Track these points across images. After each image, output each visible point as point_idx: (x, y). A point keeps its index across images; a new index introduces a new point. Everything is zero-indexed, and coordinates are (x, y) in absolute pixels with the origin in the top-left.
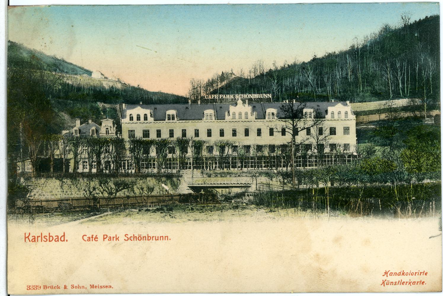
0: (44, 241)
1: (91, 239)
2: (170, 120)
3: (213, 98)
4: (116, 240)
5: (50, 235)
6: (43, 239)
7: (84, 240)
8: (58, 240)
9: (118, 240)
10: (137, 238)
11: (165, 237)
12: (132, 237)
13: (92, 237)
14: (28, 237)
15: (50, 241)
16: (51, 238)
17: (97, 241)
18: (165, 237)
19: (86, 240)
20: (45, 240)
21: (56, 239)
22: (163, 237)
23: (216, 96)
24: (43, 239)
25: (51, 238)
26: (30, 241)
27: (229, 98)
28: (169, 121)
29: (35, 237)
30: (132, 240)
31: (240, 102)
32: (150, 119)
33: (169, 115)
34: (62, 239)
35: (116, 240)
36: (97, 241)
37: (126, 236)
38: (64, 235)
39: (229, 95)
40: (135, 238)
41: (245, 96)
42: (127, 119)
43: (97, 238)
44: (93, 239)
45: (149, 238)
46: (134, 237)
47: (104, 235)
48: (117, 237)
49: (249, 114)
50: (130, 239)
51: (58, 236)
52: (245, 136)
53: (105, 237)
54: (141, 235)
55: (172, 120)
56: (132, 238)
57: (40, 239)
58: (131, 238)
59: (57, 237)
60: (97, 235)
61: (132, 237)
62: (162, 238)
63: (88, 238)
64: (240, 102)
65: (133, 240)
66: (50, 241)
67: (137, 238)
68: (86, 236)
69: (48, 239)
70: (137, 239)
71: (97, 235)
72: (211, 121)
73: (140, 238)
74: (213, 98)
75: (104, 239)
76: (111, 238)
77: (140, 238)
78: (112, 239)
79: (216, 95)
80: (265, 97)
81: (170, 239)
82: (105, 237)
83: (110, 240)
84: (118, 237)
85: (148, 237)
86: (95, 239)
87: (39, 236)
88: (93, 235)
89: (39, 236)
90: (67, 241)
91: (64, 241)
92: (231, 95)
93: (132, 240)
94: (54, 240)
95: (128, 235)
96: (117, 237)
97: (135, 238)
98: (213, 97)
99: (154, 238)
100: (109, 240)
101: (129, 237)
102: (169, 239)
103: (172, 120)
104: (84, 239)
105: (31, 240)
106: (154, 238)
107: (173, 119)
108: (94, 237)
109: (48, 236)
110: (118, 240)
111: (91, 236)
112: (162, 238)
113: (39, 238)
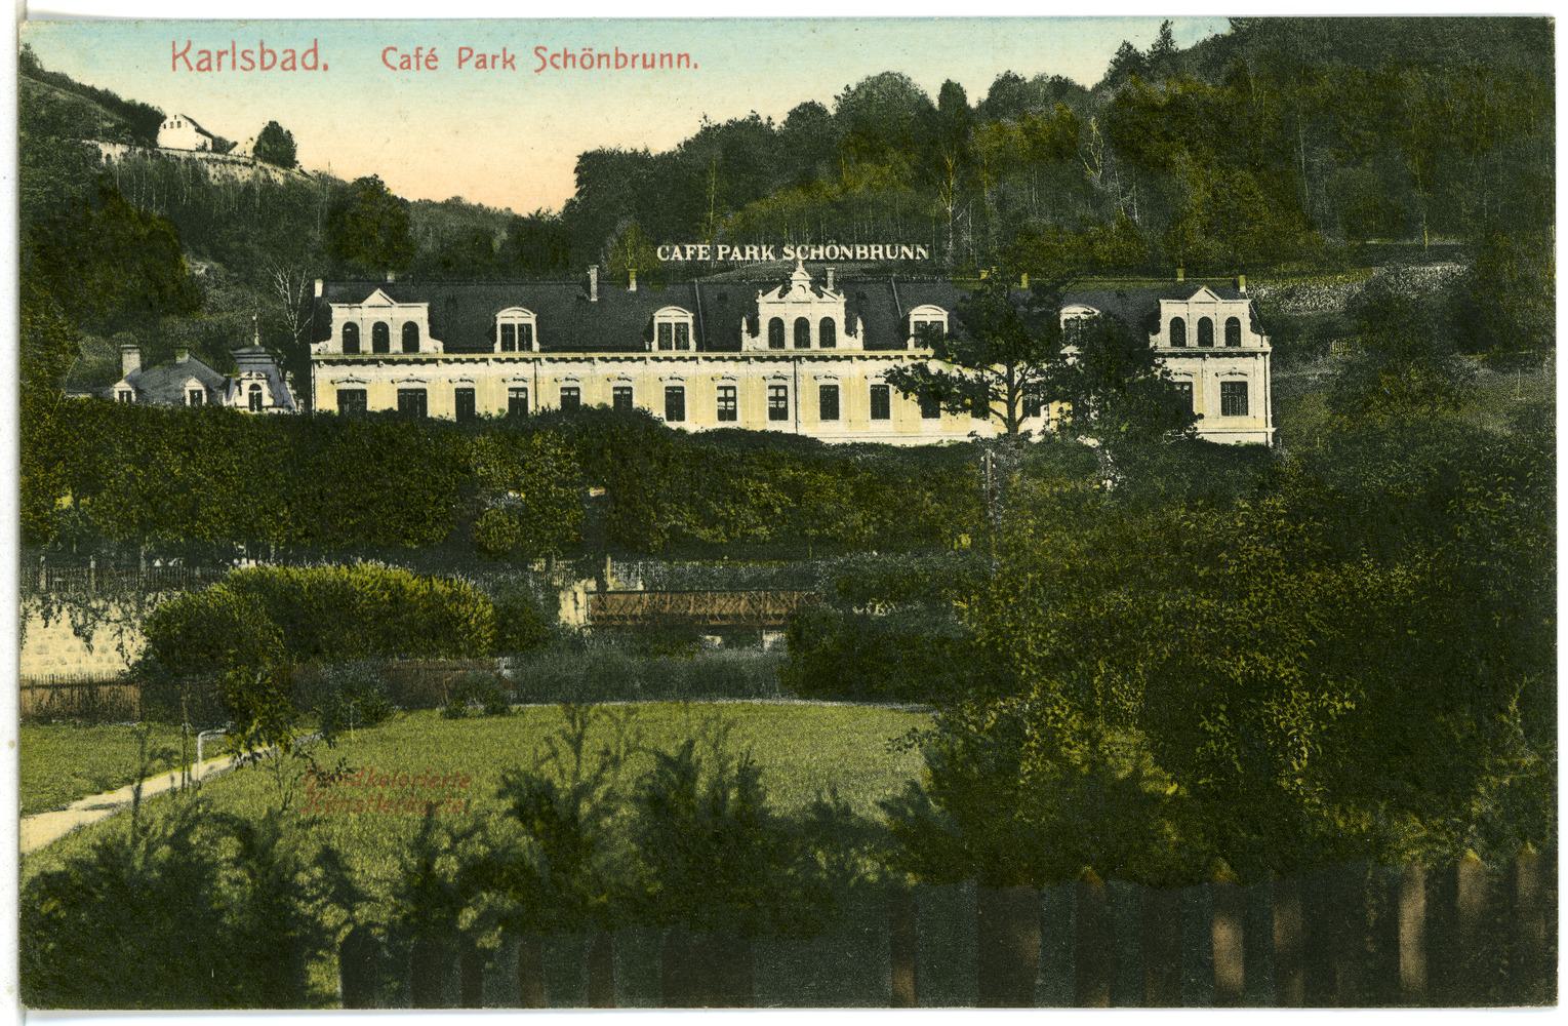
0: (243, 68)
1: (413, 61)
2: (521, 327)
3: (689, 258)
4: (504, 67)
5: (265, 48)
6: (240, 62)
7: (384, 59)
8: (294, 63)
9: (513, 68)
10: (578, 59)
11: (680, 56)
12: (558, 55)
13: (418, 56)
14: (183, 54)
15: (263, 68)
16: (268, 59)
17: (436, 68)
18: (680, 56)
19: (397, 65)
20: (248, 65)
21: (287, 60)
22: (670, 56)
23: (701, 252)
24: (240, 62)
25: (268, 59)
26: (191, 69)
27: (756, 257)
28: (509, 354)
29: (293, 51)
30: (557, 67)
31: (800, 277)
32: (428, 345)
33: (508, 329)
34: (310, 61)
35: (504, 67)
36: (436, 68)
37: (540, 51)
38: (315, 50)
39: (756, 248)
40: (570, 61)
41: (822, 252)
42: (334, 345)
43: (436, 60)
44: (422, 60)
45: (621, 61)
46: (566, 56)
47: (461, 49)
48: (508, 57)
49: (840, 327)
50: (553, 64)
51: (484, 56)
52: (824, 417)
53: (465, 53)
54: (590, 50)
55: (521, 349)
56: (559, 61)
57: (227, 60)
58: (556, 60)
59: (289, 55)
60: (433, 49)
61: (558, 55)
62: (666, 59)
63: (403, 57)
64: (800, 277)
65: (561, 64)
66: (617, 67)
67: (578, 59)
68: (395, 49)
69: (258, 65)
70: (578, 64)
71: (433, 49)
72: (681, 353)
73: (587, 62)
74: (689, 258)
75: (461, 61)
76: (484, 61)
77: (587, 62)
78: (489, 63)
79: (701, 247)
80: (903, 257)
81: (696, 66)
82: (465, 53)
83: (481, 64)
84: (513, 56)
85: (617, 55)
86: (427, 60)
87: (226, 52)
88: (421, 48)
89: (226, 52)
90: (326, 67)
91: (315, 67)
92: (764, 248)
93: (557, 67)
94: (278, 67)
95: (545, 49)
96: (508, 57)
97: (570, 61)
98: (689, 252)
99: (639, 61)
100: (477, 66)
101: (547, 55)
102: (692, 66)
103: (521, 349)
104: (389, 61)
105: (194, 64)
106: (639, 61)
107: (526, 345)
108: (425, 53)
109: (257, 50)
110: (513, 68)
111: (412, 53)
112: (666, 59)
113: (224, 57)
